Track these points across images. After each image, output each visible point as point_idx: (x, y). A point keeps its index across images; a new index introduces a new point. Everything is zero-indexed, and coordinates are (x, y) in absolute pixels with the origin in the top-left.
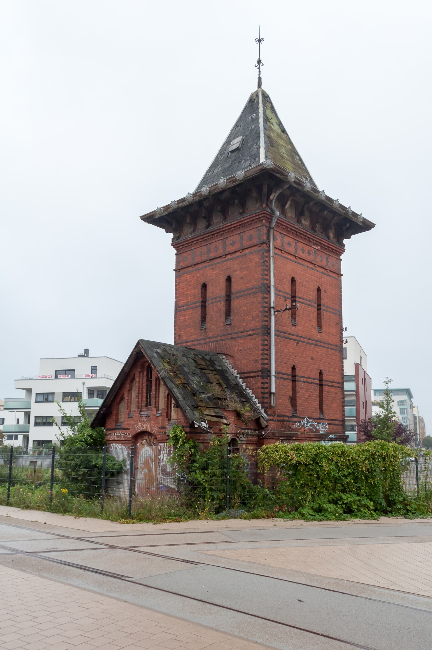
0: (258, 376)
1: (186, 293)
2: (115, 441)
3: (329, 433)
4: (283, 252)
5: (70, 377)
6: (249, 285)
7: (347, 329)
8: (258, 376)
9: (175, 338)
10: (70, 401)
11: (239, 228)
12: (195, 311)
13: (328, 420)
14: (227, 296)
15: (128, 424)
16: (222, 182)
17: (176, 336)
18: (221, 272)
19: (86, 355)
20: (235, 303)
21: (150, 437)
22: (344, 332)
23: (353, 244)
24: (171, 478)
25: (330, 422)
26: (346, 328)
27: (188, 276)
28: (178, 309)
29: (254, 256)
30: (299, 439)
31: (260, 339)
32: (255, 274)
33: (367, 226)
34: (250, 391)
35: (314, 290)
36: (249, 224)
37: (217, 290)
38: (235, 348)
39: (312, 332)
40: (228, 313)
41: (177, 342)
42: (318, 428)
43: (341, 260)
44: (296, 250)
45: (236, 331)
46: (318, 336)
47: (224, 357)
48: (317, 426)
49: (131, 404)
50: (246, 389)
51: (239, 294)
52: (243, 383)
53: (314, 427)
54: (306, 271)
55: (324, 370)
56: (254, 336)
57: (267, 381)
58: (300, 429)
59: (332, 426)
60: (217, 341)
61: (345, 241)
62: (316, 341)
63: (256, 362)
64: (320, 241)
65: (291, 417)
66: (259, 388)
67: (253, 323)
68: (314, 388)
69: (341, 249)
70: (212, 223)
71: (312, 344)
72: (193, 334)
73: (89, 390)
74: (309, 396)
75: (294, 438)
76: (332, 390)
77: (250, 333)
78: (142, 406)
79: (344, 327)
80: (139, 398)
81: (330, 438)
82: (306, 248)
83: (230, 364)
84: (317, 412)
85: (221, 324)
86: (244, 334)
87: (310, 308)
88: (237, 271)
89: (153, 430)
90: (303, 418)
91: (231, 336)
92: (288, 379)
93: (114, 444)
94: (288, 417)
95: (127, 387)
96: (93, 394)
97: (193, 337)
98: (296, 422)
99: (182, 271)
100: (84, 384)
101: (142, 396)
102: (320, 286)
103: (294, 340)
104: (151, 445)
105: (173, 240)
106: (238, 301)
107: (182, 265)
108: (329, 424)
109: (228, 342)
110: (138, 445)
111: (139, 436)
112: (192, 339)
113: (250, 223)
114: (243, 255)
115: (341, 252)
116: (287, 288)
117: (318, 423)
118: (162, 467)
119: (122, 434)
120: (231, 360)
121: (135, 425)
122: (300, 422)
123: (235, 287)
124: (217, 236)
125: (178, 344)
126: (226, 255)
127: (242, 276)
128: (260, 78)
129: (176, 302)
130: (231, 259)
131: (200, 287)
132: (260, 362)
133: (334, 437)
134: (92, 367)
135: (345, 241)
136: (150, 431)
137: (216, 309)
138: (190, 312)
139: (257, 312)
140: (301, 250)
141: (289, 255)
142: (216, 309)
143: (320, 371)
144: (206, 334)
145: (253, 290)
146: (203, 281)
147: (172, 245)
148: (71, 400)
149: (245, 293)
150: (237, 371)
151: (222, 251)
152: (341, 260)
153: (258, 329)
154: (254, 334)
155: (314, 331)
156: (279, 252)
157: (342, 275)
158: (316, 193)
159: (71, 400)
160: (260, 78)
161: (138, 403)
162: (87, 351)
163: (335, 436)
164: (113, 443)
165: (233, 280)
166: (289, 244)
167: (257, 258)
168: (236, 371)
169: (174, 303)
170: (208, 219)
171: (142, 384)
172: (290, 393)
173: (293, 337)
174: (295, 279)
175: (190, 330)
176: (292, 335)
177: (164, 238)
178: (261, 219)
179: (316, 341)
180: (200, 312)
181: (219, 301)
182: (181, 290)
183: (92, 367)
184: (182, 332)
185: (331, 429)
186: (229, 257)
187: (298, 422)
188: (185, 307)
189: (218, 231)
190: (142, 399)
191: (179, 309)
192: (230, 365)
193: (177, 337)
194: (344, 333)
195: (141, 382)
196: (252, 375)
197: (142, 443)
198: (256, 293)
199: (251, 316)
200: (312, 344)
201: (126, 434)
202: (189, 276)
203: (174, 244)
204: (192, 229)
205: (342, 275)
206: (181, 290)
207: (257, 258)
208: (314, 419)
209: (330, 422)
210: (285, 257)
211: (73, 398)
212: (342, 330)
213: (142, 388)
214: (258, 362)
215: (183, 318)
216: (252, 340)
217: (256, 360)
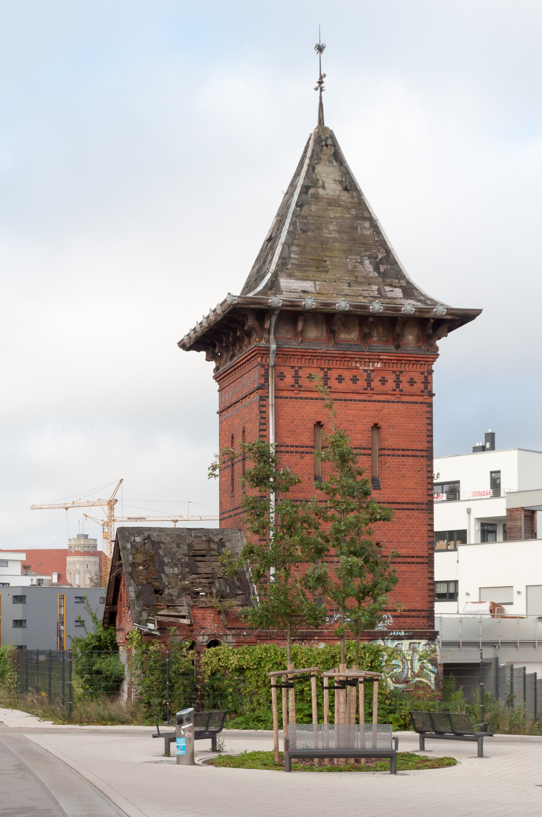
3: (391, 629)
5: (445, 498)
10: (447, 550)
19: (488, 445)
23: (448, 344)
26: (438, 474)
30: (327, 638)
33: (461, 318)
54: (347, 406)
61: (438, 343)
64: (377, 357)
73: (483, 525)
75: (316, 638)
79: (435, 472)
81: (393, 636)
82: (347, 375)
96: (495, 532)
100: (469, 511)
108: (394, 617)
115: (434, 360)
128: (321, 104)
133: (403, 634)
134: (492, 473)
135: (438, 343)
141: (310, 393)
148: (449, 547)
157: (434, 395)
158: (330, 306)
159: (449, 547)
160: (321, 104)
162: (491, 437)
163: (405, 632)
166: (310, 377)
183: (492, 473)
205: (434, 395)
210: (301, 398)
211: (452, 543)
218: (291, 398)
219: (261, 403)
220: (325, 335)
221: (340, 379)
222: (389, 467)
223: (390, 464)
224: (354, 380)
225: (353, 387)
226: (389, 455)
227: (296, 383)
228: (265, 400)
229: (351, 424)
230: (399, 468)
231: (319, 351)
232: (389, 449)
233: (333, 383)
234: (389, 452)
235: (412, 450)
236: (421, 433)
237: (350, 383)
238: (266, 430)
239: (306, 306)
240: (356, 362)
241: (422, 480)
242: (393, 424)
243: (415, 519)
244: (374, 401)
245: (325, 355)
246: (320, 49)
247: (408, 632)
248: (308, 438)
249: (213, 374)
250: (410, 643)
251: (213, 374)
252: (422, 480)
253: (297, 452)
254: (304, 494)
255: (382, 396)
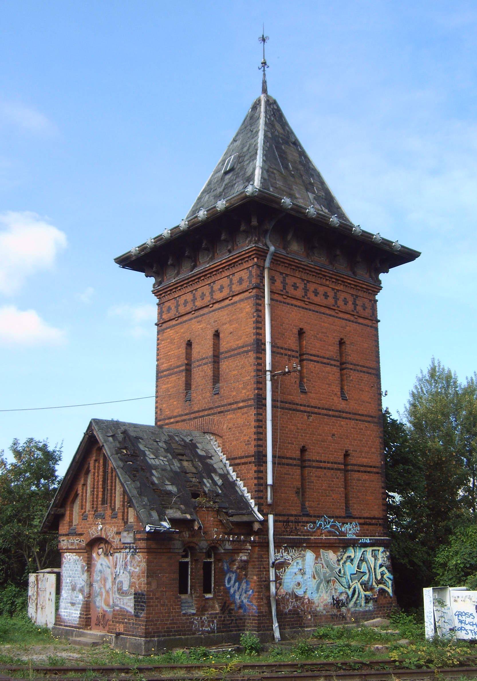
0: (250, 463)
1: (169, 353)
2: (69, 550)
4: (284, 297)
6: (240, 343)
7: (388, 393)
8: (250, 463)
9: (156, 413)
11: (228, 269)
12: (179, 377)
13: (360, 518)
14: (214, 356)
15: (82, 528)
16: (221, 205)
17: (157, 410)
18: (208, 326)
20: (224, 365)
21: (106, 545)
22: (383, 398)
23: (392, 279)
24: (128, 598)
25: (362, 521)
26: (386, 391)
27: (171, 332)
28: (159, 374)
29: (245, 305)
31: (252, 412)
32: (246, 327)
33: (408, 256)
34: (241, 482)
35: (334, 343)
36: (239, 264)
37: (203, 349)
38: (224, 426)
39: (333, 399)
40: (216, 378)
41: (158, 419)
42: (343, 529)
43: (377, 301)
44: (306, 293)
45: (225, 402)
46: (342, 405)
47: (212, 437)
48: (341, 527)
49: (86, 502)
50: (237, 480)
51: (229, 354)
52: (233, 472)
53: (337, 529)
55: (353, 451)
56: (245, 410)
57: (262, 468)
58: (315, 532)
59: (366, 527)
60: (203, 416)
61: (382, 276)
62: (340, 411)
63: (248, 443)
65: (300, 516)
66: (252, 479)
67: (244, 391)
68: (336, 475)
69: (377, 287)
70: (198, 263)
71: (333, 416)
72: (176, 407)
74: (329, 487)
75: (305, 545)
76: (365, 477)
77: (241, 404)
78: (97, 505)
79: (383, 389)
80: (93, 494)
81: (362, 543)
82: (321, 290)
83: (219, 446)
84: (342, 509)
85: (208, 394)
86: (234, 406)
87: (328, 368)
88: (226, 324)
89: (108, 536)
90: (319, 517)
91: (219, 410)
92: (295, 465)
93: (68, 554)
94: (296, 516)
95: (82, 482)
97: (176, 411)
98: (307, 522)
99: (164, 326)
101: (98, 492)
102: (342, 336)
103: (305, 412)
104: (107, 555)
105: (154, 285)
106: (227, 363)
107: (165, 317)
108: (360, 524)
109: (216, 418)
110: (94, 555)
111: (95, 542)
112: (175, 414)
113: (240, 262)
114: (232, 304)
116: (292, 342)
117: (343, 524)
118: (118, 583)
119: (76, 541)
120: (220, 441)
121: (90, 530)
122: (315, 523)
123: (224, 346)
124: (203, 279)
125: (160, 421)
126: (213, 304)
127: (232, 330)
129: (157, 366)
130: (219, 309)
131: (184, 345)
132: (253, 443)
136: (104, 537)
137: (202, 374)
138: (173, 378)
139: (249, 378)
140: (313, 292)
142: (202, 374)
143: (346, 452)
144: (191, 407)
145: (244, 349)
146: (187, 337)
147: (154, 292)
149: (236, 352)
150: (227, 457)
151: (209, 298)
152: (377, 301)
153: (250, 399)
154: (246, 407)
155: (335, 398)
156: (280, 298)
157: (379, 321)
160: (264, 83)
161: (93, 501)
164: (66, 552)
165: (221, 335)
166: (295, 287)
167: (248, 306)
168: (225, 456)
169: (155, 367)
170: (193, 259)
171: (98, 476)
172: (298, 484)
173: (302, 408)
174: (304, 330)
175: (173, 402)
176: (301, 405)
177: (143, 283)
178: (252, 257)
179: (340, 411)
180: (184, 379)
181: (205, 364)
182: (163, 350)
184: (164, 406)
185: (364, 530)
186: (216, 306)
187: (311, 522)
188: (167, 372)
189: (204, 274)
190: (97, 495)
191: (160, 375)
192: (219, 449)
193: (159, 412)
194: (383, 398)
195: (96, 474)
196: (243, 461)
197: (98, 553)
198: (247, 352)
199: (242, 382)
200: (333, 416)
201: (80, 542)
202: (173, 331)
203: (155, 291)
204: (176, 272)
205: (379, 321)
206: (163, 350)
207: (248, 306)
208: (337, 517)
209: (362, 521)
210: (288, 304)
212: (380, 394)
213: (98, 482)
214: (250, 444)
215: (166, 386)
216: (243, 414)
217: (248, 441)
218: (280, 302)
219: (258, 301)
220: (303, 250)
221: (316, 293)
222: (352, 380)
223: (353, 378)
224: (326, 296)
225: (325, 302)
226: (351, 369)
227: (284, 289)
228: (261, 300)
229: (324, 336)
230: (359, 382)
231: (302, 263)
232: (351, 364)
233: (311, 295)
234: (351, 367)
235: (367, 367)
236: (372, 353)
237: (323, 297)
238: (263, 328)
239: (309, 214)
240: (327, 280)
241: (374, 396)
242: (353, 341)
243: (371, 431)
244: (340, 318)
245: (306, 268)
246: (264, 40)
247: (372, 539)
248: (294, 343)
249: (152, 289)
250: (372, 550)
251: (152, 289)
252: (374, 396)
253: (286, 355)
254: (292, 397)
255: (345, 314)
